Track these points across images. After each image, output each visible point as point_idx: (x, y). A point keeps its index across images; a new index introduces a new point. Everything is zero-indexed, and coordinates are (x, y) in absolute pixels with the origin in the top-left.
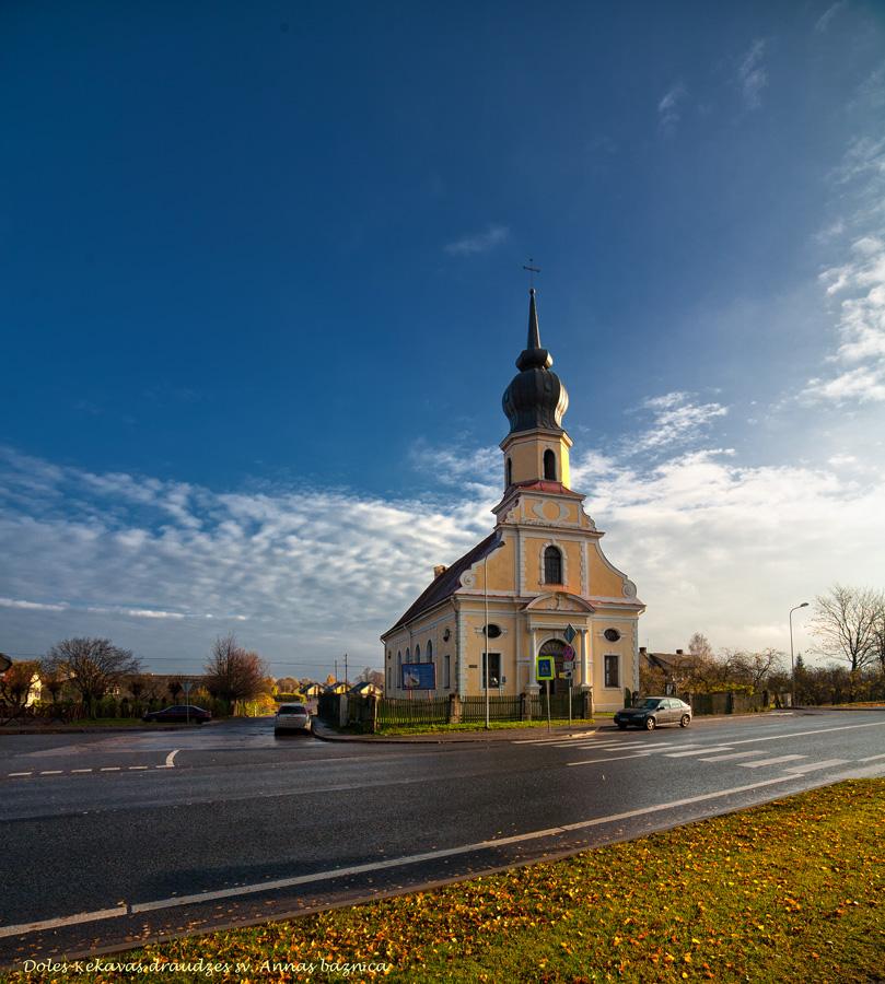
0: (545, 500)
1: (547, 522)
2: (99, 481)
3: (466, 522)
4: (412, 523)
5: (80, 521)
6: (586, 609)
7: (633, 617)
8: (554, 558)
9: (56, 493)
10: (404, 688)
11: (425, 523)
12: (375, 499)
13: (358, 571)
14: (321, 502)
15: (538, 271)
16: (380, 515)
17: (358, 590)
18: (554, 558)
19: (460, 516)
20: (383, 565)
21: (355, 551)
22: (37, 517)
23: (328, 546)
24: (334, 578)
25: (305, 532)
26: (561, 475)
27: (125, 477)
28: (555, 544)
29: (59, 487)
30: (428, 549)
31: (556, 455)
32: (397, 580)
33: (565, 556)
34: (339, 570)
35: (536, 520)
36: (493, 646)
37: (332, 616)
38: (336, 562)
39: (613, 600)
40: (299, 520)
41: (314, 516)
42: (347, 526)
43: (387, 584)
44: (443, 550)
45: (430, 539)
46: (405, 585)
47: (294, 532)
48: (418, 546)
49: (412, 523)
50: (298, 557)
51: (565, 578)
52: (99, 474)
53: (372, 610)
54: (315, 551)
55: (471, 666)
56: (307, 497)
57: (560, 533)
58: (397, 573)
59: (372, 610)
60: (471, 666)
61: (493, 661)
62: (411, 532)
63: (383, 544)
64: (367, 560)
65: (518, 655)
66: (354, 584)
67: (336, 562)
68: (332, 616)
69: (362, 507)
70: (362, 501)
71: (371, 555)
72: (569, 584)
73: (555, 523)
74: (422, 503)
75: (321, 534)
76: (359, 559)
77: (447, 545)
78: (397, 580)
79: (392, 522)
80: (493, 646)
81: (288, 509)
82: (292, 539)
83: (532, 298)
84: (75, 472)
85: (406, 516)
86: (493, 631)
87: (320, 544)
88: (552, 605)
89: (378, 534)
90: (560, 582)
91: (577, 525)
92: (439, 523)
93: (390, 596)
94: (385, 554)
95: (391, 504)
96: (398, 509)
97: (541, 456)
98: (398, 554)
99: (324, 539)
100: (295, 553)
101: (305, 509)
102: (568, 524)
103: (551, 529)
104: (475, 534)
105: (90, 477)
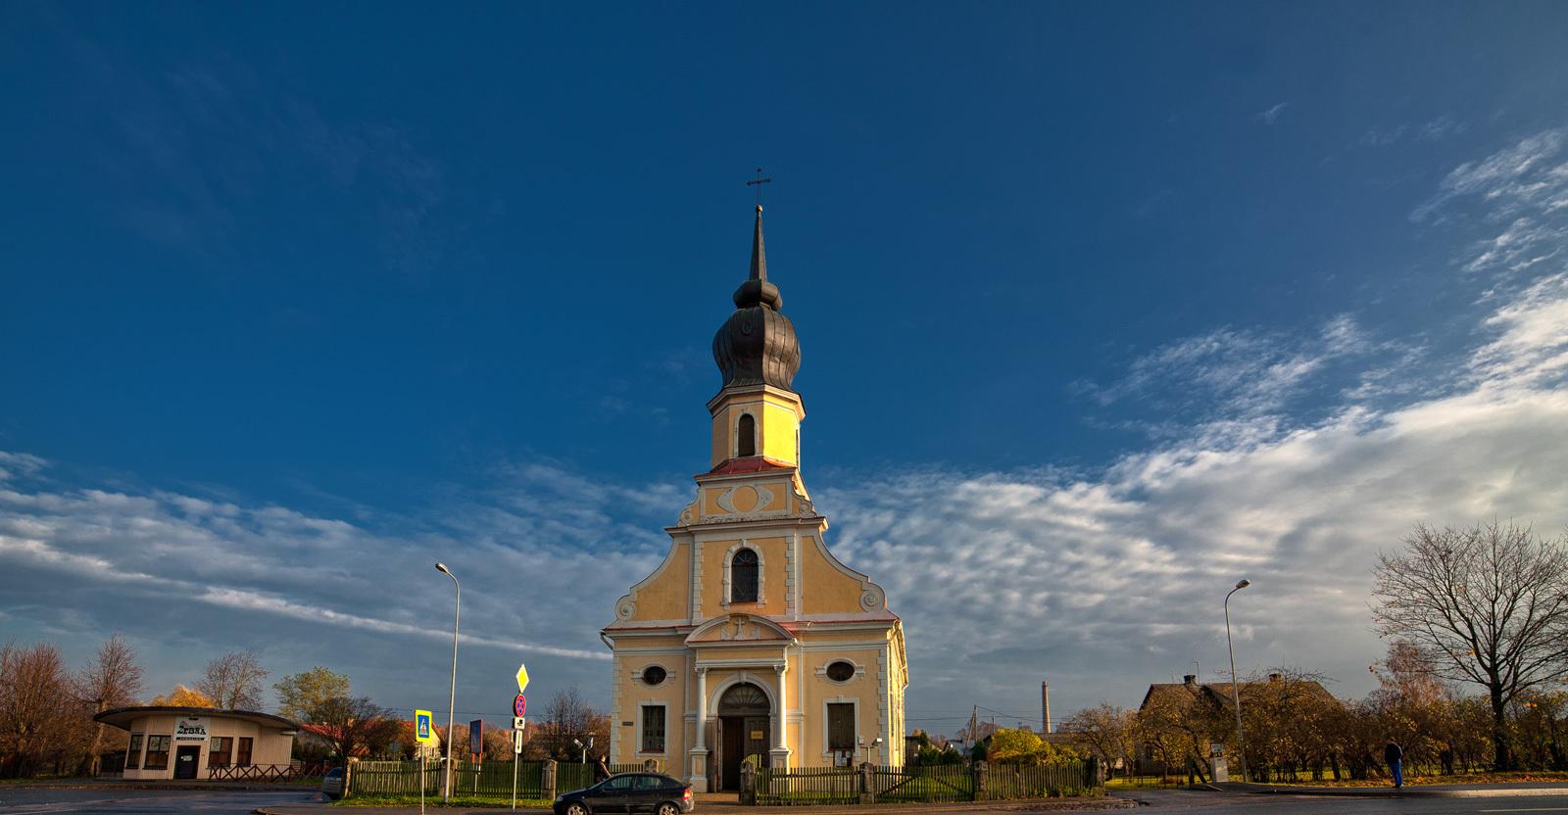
0: (735, 486)
1: (737, 515)
2: (641, 497)
3: (1127, 486)
4: (1041, 501)
5: (636, 551)
6: (780, 636)
7: (880, 640)
8: (746, 566)
9: (605, 520)
10: (150, 736)
11: (1062, 498)
12: (985, 471)
13: (973, 581)
14: (913, 486)
15: (769, 181)
16: (996, 495)
17: (977, 608)
18: (746, 566)
19: (1114, 482)
20: (1009, 568)
21: (965, 553)
22: (592, 552)
23: (928, 550)
24: (941, 595)
25: (897, 532)
26: (762, 447)
27: (666, 488)
28: (746, 545)
29: (606, 510)
30: (1072, 535)
31: (756, 420)
32: (1029, 590)
33: (762, 561)
34: (947, 582)
35: (722, 517)
36: (655, 696)
37: (945, 649)
38: (942, 572)
39: (843, 617)
40: (886, 518)
41: (902, 513)
42: (950, 518)
43: (1015, 596)
44: (1095, 534)
45: (1073, 521)
46: (1042, 595)
47: (884, 535)
48: (1057, 533)
49: (1041, 501)
50: (891, 571)
51: (762, 595)
52: (641, 489)
53: (998, 636)
54: (913, 558)
55: (625, 724)
56: (892, 484)
57: (754, 529)
58: (1028, 578)
59: (998, 636)
60: (625, 724)
61: (654, 716)
62: (1043, 513)
63: (1004, 537)
64: (985, 563)
65: (687, 708)
66: (970, 601)
67: (942, 572)
68: (945, 649)
69: (972, 485)
70: (969, 477)
71: (991, 555)
72: (765, 606)
73: (749, 515)
74: (1056, 466)
75: (918, 534)
76: (973, 563)
77: (1099, 527)
78: (1029, 590)
79: (1015, 503)
80: (655, 696)
81: (869, 504)
82: (882, 547)
83: (758, 218)
84: (615, 488)
85: (1034, 491)
86: (654, 675)
87: (917, 549)
88: (726, 634)
89: (997, 523)
90: (753, 598)
91: (783, 512)
92: (1083, 495)
93: (1022, 615)
94: (1010, 552)
95: (1008, 476)
96: (1023, 483)
97: (734, 424)
98: (1028, 548)
99: (921, 541)
100: (886, 565)
101: (892, 501)
102: (769, 514)
103: (743, 525)
104: (1143, 504)
105: (631, 493)
